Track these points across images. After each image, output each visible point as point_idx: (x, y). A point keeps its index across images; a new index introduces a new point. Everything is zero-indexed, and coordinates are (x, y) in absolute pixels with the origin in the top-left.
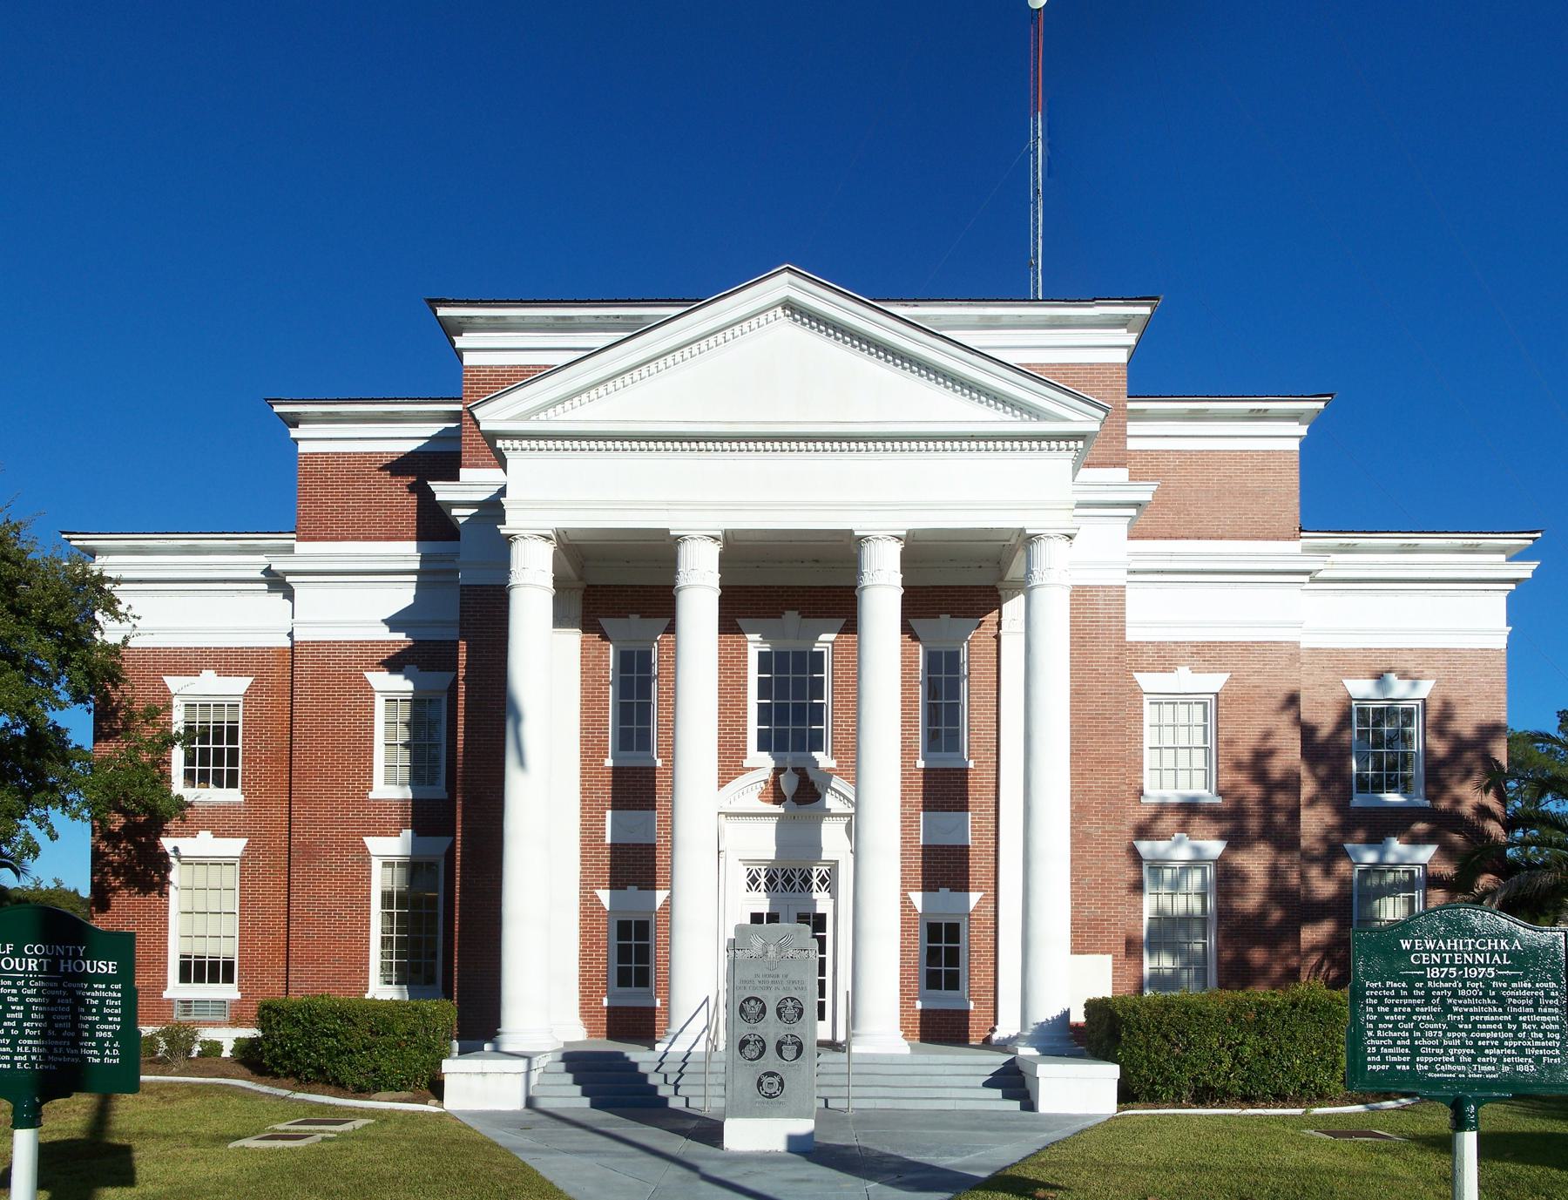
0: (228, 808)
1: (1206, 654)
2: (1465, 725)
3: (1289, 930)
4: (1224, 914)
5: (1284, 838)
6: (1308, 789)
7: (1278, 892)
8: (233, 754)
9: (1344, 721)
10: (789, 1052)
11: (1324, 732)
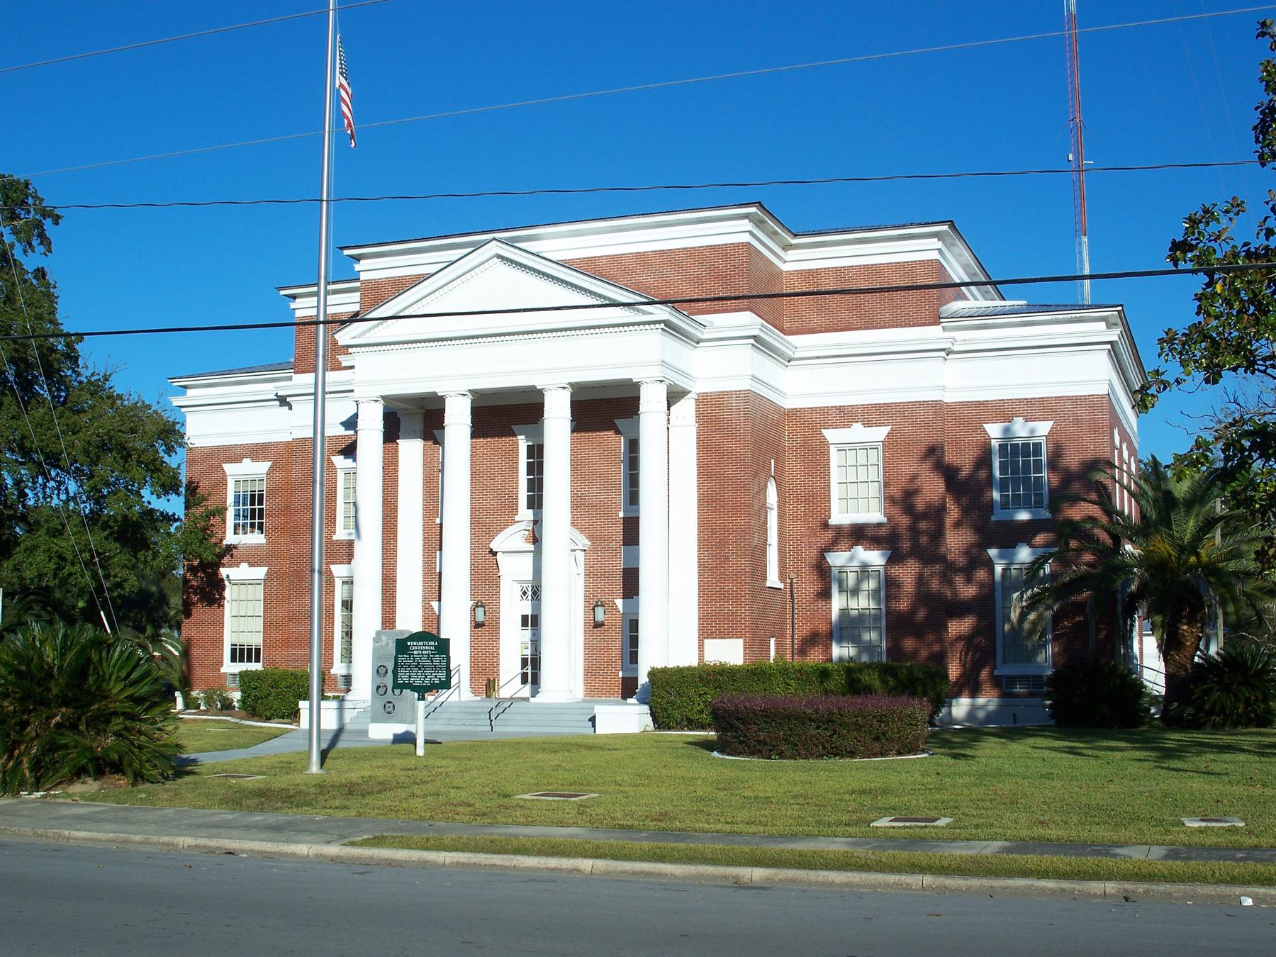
0: (257, 547)
1: (871, 414)
2: (1072, 460)
3: (938, 626)
5: (928, 552)
6: (953, 513)
7: (923, 595)
8: (261, 511)
9: (984, 460)
11: (965, 473)
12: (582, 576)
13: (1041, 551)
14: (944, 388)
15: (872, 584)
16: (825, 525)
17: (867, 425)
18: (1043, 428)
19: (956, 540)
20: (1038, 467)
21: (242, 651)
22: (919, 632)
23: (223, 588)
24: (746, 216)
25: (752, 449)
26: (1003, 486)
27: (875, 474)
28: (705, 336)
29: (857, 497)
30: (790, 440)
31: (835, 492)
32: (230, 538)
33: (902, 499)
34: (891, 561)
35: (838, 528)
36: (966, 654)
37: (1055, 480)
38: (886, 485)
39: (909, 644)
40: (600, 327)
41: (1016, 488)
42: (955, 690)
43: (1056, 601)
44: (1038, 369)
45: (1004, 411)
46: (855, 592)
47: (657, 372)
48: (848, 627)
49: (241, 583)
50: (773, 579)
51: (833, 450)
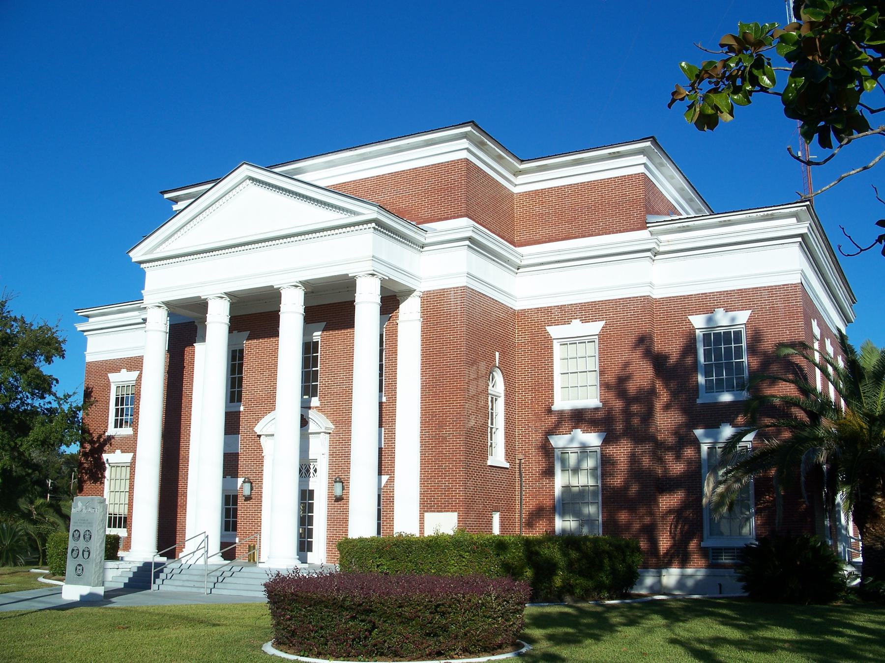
1: (587, 311)
2: (768, 345)
4: (604, 487)
6: (664, 396)
7: (636, 472)
9: (690, 347)
10: (86, 554)
11: (673, 360)
12: (327, 456)
13: (739, 430)
14: (651, 285)
15: (590, 463)
16: (549, 411)
17: (585, 320)
18: (743, 317)
19: (665, 421)
20: (739, 355)
21: (120, 518)
22: (631, 505)
23: (104, 469)
24: (465, 136)
25: (477, 343)
26: (707, 373)
27: (593, 364)
28: (428, 241)
29: (576, 384)
30: (520, 337)
31: (558, 381)
32: (111, 431)
33: (616, 385)
34: (606, 442)
35: (561, 413)
36: (676, 527)
37: (755, 363)
38: (602, 373)
39: (623, 517)
40: (323, 230)
41: (719, 373)
42: (666, 560)
43: (746, 473)
44: (739, 262)
45: (706, 303)
46: (576, 470)
47: (369, 267)
48: (570, 502)
49: (116, 466)
50: (498, 457)
51: (556, 345)
